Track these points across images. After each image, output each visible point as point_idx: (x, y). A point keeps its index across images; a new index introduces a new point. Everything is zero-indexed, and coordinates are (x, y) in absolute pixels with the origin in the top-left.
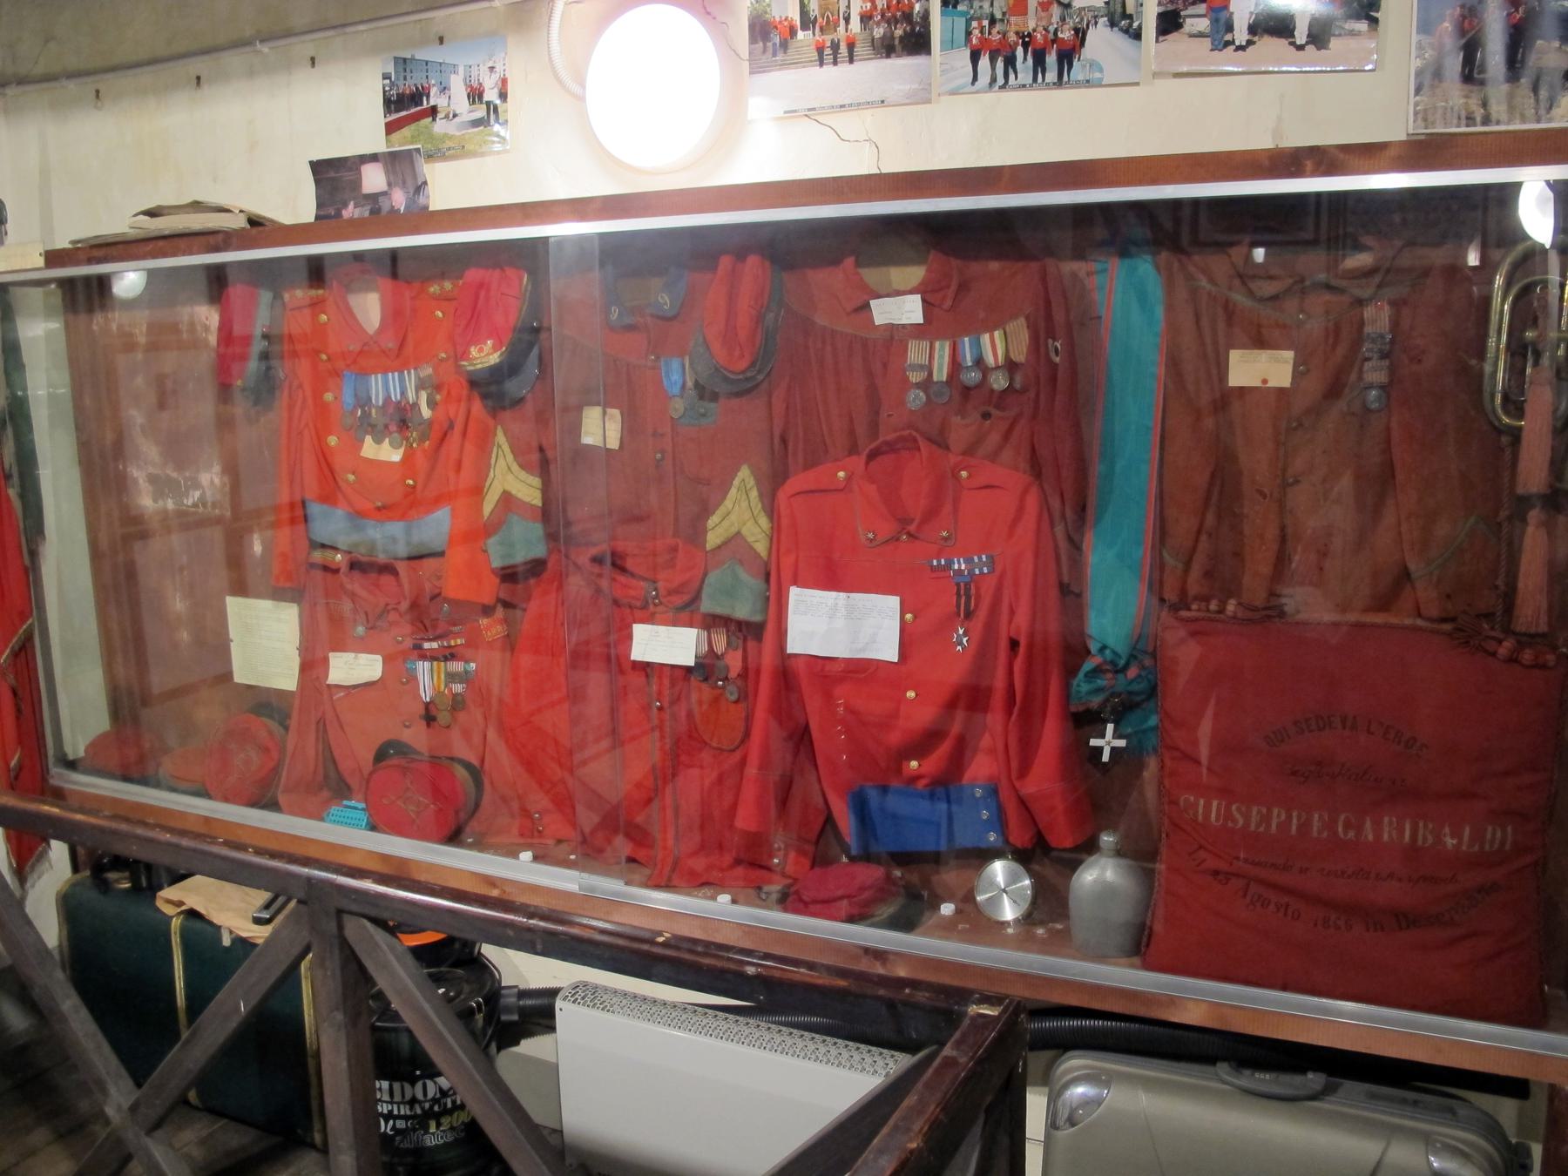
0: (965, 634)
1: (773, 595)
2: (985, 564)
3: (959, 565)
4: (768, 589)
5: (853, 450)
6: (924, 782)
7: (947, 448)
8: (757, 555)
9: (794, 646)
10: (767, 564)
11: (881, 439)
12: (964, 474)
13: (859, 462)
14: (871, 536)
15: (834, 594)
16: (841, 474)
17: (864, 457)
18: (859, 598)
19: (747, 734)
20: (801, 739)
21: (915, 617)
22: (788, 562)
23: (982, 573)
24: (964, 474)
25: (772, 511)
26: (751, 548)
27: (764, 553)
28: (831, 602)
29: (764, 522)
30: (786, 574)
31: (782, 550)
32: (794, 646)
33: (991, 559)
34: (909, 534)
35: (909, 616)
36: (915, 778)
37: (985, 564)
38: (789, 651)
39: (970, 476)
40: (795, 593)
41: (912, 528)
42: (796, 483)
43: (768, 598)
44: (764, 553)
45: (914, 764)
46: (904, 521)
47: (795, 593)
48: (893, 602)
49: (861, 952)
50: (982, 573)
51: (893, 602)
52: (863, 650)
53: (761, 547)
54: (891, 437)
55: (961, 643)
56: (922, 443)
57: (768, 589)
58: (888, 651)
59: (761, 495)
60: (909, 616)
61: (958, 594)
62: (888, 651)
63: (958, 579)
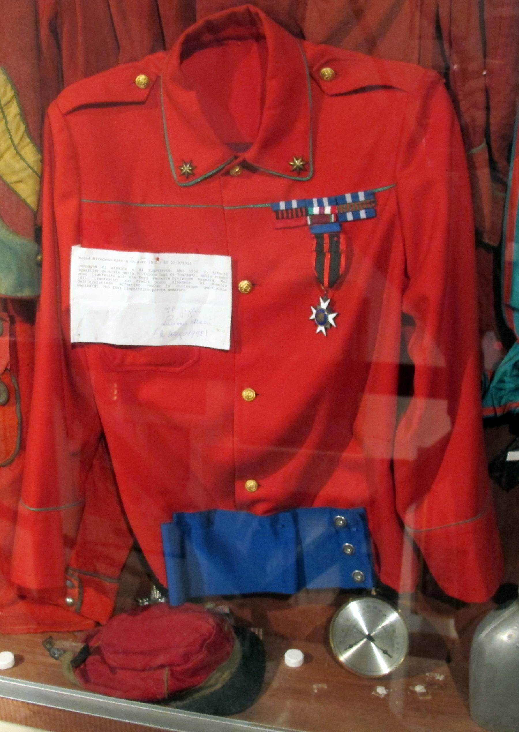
0: (331, 309)
1: (46, 257)
2: (362, 205)
3: (321, 208)
4: (40, 252)
5: (160, 41)
6: (261, 507)
7: (301, 35)
8: (21, 202)
9: (81, 331)
10: (36, 214)
11: (200, 23)
12: (327, 71)
13: (168, 60)
14: (187, 168)
15: (135, 255)
16: (141, 79)
17: (177, 48)
18: (170, 259)
19: (23, 446)
20: (96, 448)
21: (253, 285)
22: (66, 211)
23: (357, 219)
24: (327, 71)
25: (38, 131)
26: (12, 192)
27: (31, 200)
28: (132, 267)
29: (30, 153)
30: (66, 228)
31: (57, 194)
32: (81, 331)
33: (371, 196)
34: (245, 166)
35: (244, 284)
36: (252, 503)
37: (362, 205)
38: (74, 338)
39: (336, 74)
40: (79, 255)
41: (249, 155)
42: (68, 97)
43: (40, 264)
44: (31, 200)
45: (251, 484)
46: (236, 147)
47: (79, 255)
48: (222, 264)
49: (39, 225)
50: (357, 219)
51: (222, 264)
52: (176, 335)
53: (27, 191)
54: (215, 16)
55: (324, 322)
56: (268, 28)
57: (40, 252)
58: (216, 335)
59: (24, 114)
60: (244, 284)
61: (320, 252)
62: (216, 335)
63: (318, 229)
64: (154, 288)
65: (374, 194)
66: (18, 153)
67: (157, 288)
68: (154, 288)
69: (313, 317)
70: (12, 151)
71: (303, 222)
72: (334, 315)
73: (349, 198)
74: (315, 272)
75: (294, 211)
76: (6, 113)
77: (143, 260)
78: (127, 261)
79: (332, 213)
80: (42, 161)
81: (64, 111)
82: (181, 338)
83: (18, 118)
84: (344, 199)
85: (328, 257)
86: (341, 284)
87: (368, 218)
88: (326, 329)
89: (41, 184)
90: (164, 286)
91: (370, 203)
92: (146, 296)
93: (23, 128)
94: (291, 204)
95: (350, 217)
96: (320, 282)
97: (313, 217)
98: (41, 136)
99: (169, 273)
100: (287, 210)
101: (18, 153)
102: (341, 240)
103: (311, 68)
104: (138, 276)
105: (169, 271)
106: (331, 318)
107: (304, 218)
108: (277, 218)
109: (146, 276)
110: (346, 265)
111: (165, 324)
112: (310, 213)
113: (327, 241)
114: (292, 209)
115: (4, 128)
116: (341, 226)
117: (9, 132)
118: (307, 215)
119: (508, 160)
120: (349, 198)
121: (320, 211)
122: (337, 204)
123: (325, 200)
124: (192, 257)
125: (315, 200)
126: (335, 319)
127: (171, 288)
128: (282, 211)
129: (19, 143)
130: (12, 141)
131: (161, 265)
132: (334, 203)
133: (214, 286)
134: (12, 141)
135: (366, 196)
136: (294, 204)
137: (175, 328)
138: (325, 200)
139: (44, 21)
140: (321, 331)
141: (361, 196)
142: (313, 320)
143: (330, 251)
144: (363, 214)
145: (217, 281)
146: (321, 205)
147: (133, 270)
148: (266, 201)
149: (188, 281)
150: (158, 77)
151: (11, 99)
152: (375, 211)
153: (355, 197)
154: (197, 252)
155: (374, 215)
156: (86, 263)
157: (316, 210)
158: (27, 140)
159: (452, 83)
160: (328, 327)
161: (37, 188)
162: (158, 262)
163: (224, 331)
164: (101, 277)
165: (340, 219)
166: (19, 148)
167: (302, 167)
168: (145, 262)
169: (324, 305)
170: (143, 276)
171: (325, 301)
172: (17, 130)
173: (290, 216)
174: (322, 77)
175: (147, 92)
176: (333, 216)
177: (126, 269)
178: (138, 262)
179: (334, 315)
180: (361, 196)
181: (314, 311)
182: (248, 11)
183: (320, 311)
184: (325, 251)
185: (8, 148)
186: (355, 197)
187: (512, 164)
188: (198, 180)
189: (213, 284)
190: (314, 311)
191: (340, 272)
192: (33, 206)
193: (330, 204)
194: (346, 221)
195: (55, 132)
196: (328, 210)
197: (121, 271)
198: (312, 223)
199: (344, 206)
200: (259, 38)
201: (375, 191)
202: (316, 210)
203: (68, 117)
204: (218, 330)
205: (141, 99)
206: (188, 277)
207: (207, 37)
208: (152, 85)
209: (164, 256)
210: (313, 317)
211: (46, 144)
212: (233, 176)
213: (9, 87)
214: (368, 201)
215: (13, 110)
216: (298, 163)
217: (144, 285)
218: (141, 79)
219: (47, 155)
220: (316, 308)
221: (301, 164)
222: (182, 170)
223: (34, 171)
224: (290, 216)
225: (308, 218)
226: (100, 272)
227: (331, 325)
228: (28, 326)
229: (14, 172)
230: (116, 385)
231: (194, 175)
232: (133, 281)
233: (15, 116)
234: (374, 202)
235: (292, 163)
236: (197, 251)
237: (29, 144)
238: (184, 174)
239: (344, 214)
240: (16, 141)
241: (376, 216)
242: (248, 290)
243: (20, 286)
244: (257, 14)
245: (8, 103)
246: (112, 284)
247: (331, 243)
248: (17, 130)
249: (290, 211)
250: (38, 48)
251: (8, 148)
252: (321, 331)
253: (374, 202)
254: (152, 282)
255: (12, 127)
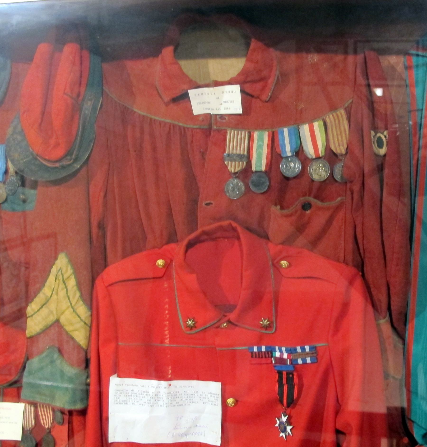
0: (289, 422)
1: (93, 380)
7: (267, 238)
12: (284, 263)
14: (190, 323)
15: (154, 383)
16: (160, 262)
23: (305, 363)
24: (284, 263)
28: (152, 391)
29: (83, 310)
35: (230, 401)
39: (290, 265)
40: (115, 382)
47: (115, 382)
48: (214, 388)
50: (305, 363)
51: (214, 388)
52: (183, 435)
55: (284, 431)
59: (79, 285)
61: (281, 385)
63: (279, 367)
64: (168, 405)
65: (315, 348)
66: (74, 311)
67: (169, 405)
68: (168, 405)
69: (277, 425)
70: (71, 310)
71: (269, 361)
72: (291, 427)
73: (299, 349)
74: (278, 395)
75: (263, 353)
76: (67, 284)
77: (160, 386)
78: (149, 387)
79: (288, 358)
80: (91, 316)
81: (107, 284)
82: (187, 437)
83: (75, 288)
84: (296, 350)
85: (286, 387)
86: (296, 404)
87: (312, 363)
88: (286, 435)
89: (90, 331)
90: (174, 403)
91: (313, 354)
92: (161, 411)
93: (78, 294)
94: (261, 348)
95: (300, 361)
96: (281, 402)
97: (276, 358)
98: (91, 300)
99: (178, 394)
100: (259, 352)
101: (74, 311)
102: (295, 377)
103: (273, 260)
104: (156, 396)
105: (178, 392)
106: (289, 428)
107: (270, 359)
108: (252, 357)
109: (162, 397)
110: (298, 393)
111: (175, 428)
112: (274, 355)
113: (285, 376)
114: (262, 352)
115: (65, 294)
116: (294, 367)
117: (69, 298)
118: (272, 357)
119: (405, 325)
120: (299, 349)
121: (280, 355)
122: (291, 353)
123: (284, 349)
124: (194, 383)
125: (277, 348)
126: (291, 430)
127: (179, 404)
128: (255, 353)
129: (75, 305)
130: (71, 303)
131: (172, 389)
132: (290, 352)
133: (209, 402)
134: (71, 303)
135: (310, 348)
136: (264, 349)
137: (183, 431)
138: (284, 349)
139: (95, 224)
140: (282, 436)
141: (307, 349)
142: (277, 427)
143: (287, 384)
144: (308, 360)
145: (212, 399)
146: (281, 351)
147: (153, 393)
148: (245, 345)
149: (192, 398)
150: (172, 260)
151: (71, 274)
152: (317, 359)
153: (303, 349)
154: (198, 379)
155: (316, 361)
156: (120, 388)
157: (278, 354)
158: (81, 302)
159: (366, 276)
160: (287, 434)
161: (88, 334)
162: (171, 387)
163: (216, 433)
164: (131, 397)
165: (294, 363)
166: (75, 308)
167: (268, 325)
168: (161, 387)
169: (284, 419)
170: (160, 396)
171: (285, 416)
172: (74, 297)
173: (261, 356)
174: (281, 266)
175: (165, 269)
176: (289, 360)
177: (148, 392)
178: (156, 387)
179: (291, 427)
180: (307, 349)
181: (278, 422)
182: (230, 224)
183: (281, 423)
184: (284, 383)
185: (68, 307)
186: (303, 349)
187: (407, 327)
188: (199, 330)
189: (208, 401)
190: (278, 422)
191: (295, 398)
192: (85, 347)
193: (287, 351)
194: (298, 364)
195: (100, 297)
196: (285, 356)
197: (145, 394)
198: (275, 363)
199: (295, 354)
200: (238, 238)
201: (318, 345)
202: (278, 354)
203: (109, 288)
204: (213, 432)
205: (160, 275)
206: (192, 396)
207: (204, 237)
208: (167, 266)
209: (174, 383)
210: (277, 425)
211: (94, 304)
212: (222, 328)
213: (69, 267)
214: (311, 352)
215: (72, 283)
216: (265, 322)
217: (160, 403)
218: (160, 262)
219: (95, 313)
220: (279, 420)
221: (268, 323)
222: (187, 324)
223: (85, 323)
224: (261, 356)
225: (273, 359)
226: (130, 394)
227: (289, 433)
228: (81, 418)
229: (72, 324)
230: (170, 368)
231: (195, 327)
232: (153, 400)
233: (73, 287)
234: (315, 353)
235: (261, 323)
236: (198, 378)
237: (82, 305)
238: (189, 326)
239: (297, 360)
240: (73, 303)
241: (317, 362)
242: (233, 405)
243: (74, 402)
244: (236, 227)
245: (68, 278)
246: (138, 402)
247: (287, 378)
248: (74, 297)
249: (260, 353)
250: (91, 238)
251: (68, 307)
252: (282, 436)
253: (315, 353)
254: (166, 401)
255: (71, 294)
